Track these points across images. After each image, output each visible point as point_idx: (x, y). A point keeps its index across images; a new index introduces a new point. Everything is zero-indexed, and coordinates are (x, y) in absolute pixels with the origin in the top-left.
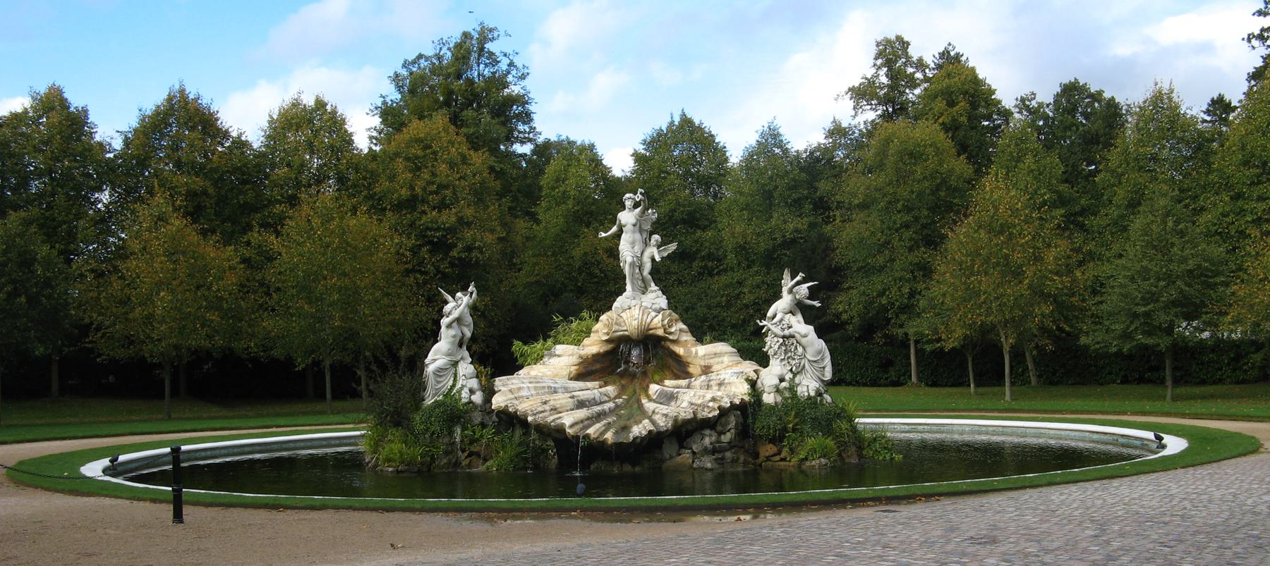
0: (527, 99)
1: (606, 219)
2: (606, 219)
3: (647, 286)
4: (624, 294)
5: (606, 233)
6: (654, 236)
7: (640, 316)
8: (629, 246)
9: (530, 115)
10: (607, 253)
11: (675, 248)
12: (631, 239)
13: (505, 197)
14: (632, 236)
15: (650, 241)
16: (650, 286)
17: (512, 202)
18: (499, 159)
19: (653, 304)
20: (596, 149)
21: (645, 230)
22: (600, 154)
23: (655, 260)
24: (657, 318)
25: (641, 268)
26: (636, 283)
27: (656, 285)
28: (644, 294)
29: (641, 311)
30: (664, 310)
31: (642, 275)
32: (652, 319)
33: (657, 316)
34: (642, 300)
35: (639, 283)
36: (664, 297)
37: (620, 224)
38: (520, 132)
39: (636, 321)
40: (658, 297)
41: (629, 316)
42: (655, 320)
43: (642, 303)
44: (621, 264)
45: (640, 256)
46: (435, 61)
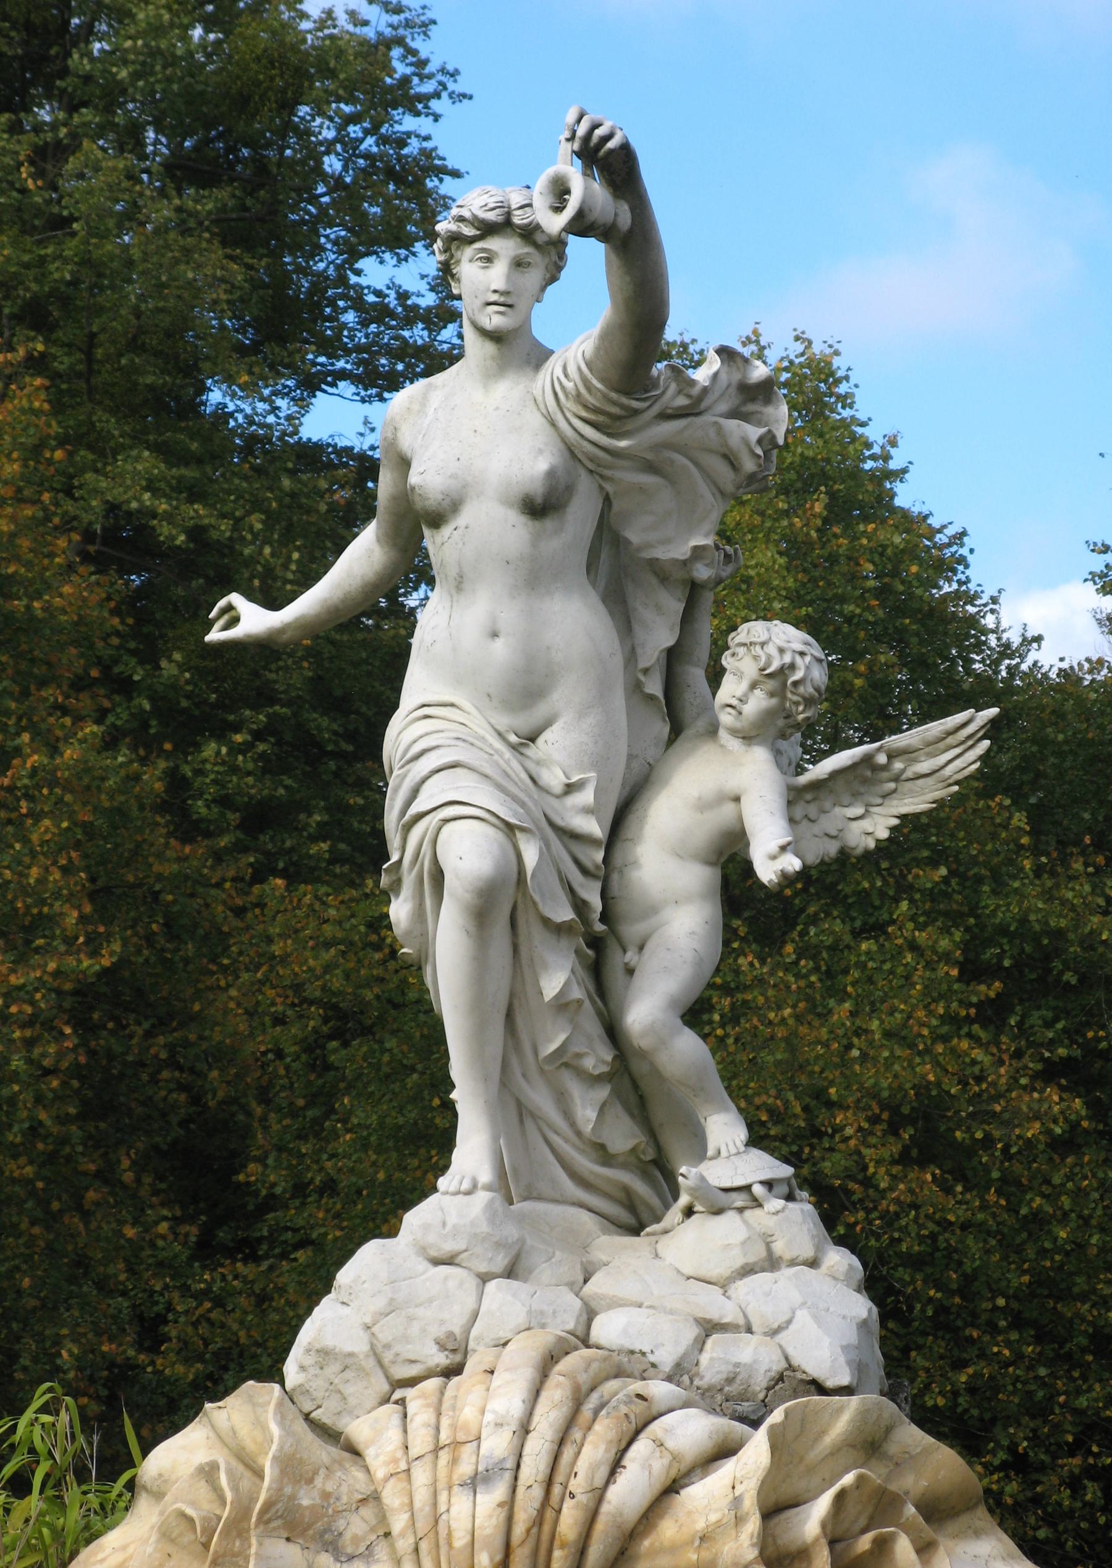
0: (401, 69)
1: (904, 889)
2: (904, 889)
3: (674, 1146)
4: (414, 1219)
5: (273, 603)
6: (754, 630)
7: (537, 1450)
8: (479, 725)
9: (419, 182)
10: (894, 1129)
11: (969, 761)
12: (500, 649)
13: (221, 732)
14: (509, 615)
15: (716, 676)
16: (699, 1151)
17: (269, 767)
18: (190, 473)
19: (710, 1328)
20: (846, 400)
21: (661, 572)
22: (874, 433)
23: (748, 869)
24: (728, 1469)
25: (616, 960)
26: (541, 1099)
27: (757, 1139)
28: (636, 1230)
29: (556, 1394)
30: (820, 1389)
31: (613, 1031)
32: (672, 1488)
33: (725, 1451)
34: (597, 1285)
35: (587, 1114)
36: (839, 1259)
37: (405, 497)
38: (379, 313)
39: (490, 1499)
40: (772, 1263)
41: (420, 1442)
42: (614, 1493)
43: (590, 1314)
44: (400, 911)
45: (594, 828)
46: (803, 611)
